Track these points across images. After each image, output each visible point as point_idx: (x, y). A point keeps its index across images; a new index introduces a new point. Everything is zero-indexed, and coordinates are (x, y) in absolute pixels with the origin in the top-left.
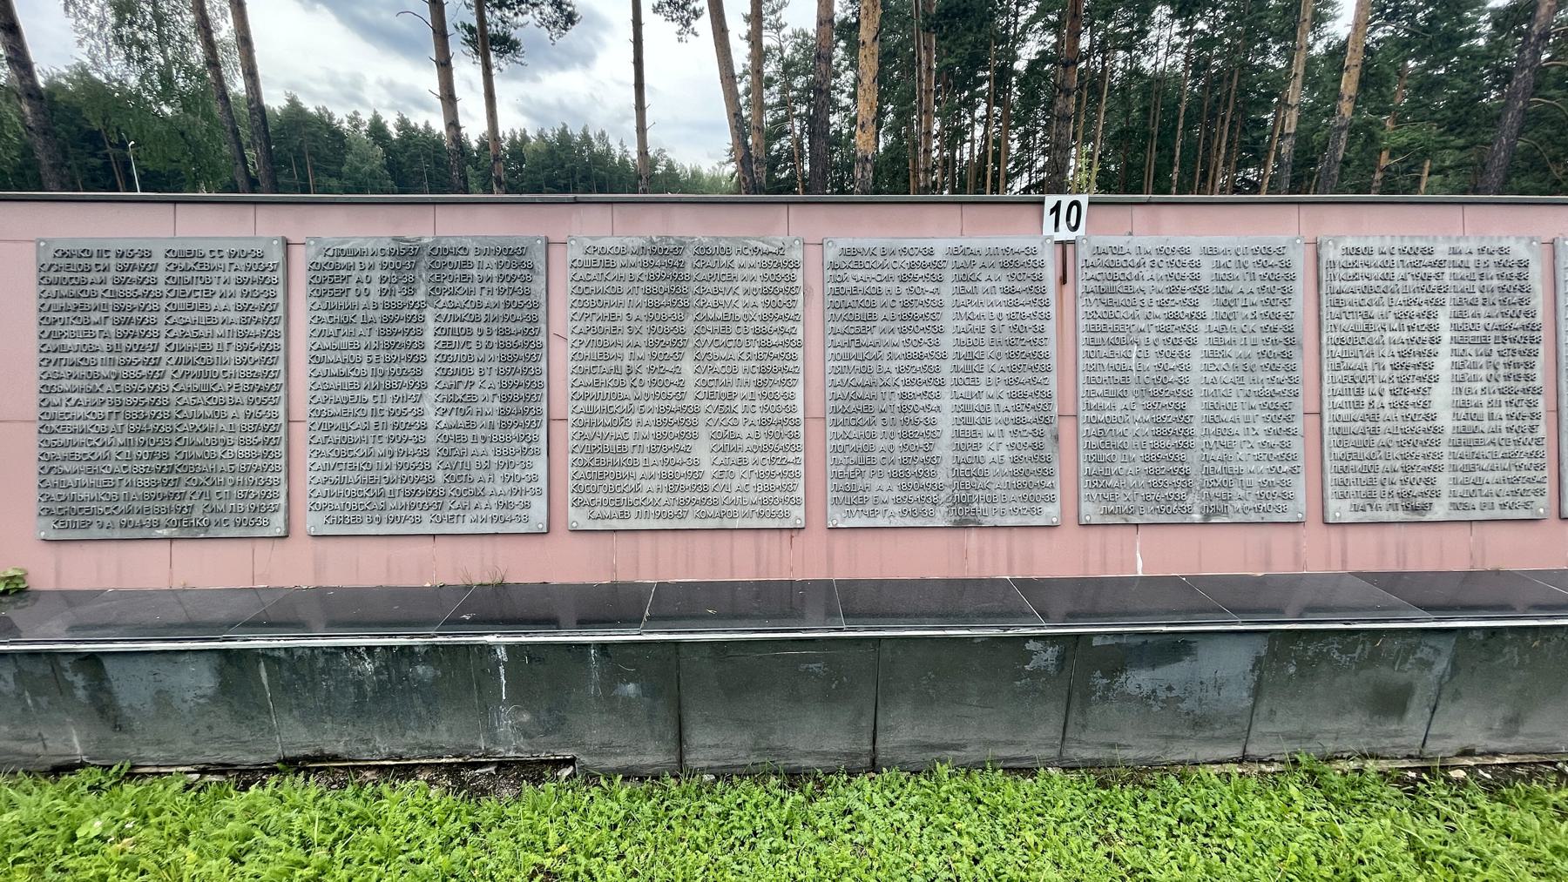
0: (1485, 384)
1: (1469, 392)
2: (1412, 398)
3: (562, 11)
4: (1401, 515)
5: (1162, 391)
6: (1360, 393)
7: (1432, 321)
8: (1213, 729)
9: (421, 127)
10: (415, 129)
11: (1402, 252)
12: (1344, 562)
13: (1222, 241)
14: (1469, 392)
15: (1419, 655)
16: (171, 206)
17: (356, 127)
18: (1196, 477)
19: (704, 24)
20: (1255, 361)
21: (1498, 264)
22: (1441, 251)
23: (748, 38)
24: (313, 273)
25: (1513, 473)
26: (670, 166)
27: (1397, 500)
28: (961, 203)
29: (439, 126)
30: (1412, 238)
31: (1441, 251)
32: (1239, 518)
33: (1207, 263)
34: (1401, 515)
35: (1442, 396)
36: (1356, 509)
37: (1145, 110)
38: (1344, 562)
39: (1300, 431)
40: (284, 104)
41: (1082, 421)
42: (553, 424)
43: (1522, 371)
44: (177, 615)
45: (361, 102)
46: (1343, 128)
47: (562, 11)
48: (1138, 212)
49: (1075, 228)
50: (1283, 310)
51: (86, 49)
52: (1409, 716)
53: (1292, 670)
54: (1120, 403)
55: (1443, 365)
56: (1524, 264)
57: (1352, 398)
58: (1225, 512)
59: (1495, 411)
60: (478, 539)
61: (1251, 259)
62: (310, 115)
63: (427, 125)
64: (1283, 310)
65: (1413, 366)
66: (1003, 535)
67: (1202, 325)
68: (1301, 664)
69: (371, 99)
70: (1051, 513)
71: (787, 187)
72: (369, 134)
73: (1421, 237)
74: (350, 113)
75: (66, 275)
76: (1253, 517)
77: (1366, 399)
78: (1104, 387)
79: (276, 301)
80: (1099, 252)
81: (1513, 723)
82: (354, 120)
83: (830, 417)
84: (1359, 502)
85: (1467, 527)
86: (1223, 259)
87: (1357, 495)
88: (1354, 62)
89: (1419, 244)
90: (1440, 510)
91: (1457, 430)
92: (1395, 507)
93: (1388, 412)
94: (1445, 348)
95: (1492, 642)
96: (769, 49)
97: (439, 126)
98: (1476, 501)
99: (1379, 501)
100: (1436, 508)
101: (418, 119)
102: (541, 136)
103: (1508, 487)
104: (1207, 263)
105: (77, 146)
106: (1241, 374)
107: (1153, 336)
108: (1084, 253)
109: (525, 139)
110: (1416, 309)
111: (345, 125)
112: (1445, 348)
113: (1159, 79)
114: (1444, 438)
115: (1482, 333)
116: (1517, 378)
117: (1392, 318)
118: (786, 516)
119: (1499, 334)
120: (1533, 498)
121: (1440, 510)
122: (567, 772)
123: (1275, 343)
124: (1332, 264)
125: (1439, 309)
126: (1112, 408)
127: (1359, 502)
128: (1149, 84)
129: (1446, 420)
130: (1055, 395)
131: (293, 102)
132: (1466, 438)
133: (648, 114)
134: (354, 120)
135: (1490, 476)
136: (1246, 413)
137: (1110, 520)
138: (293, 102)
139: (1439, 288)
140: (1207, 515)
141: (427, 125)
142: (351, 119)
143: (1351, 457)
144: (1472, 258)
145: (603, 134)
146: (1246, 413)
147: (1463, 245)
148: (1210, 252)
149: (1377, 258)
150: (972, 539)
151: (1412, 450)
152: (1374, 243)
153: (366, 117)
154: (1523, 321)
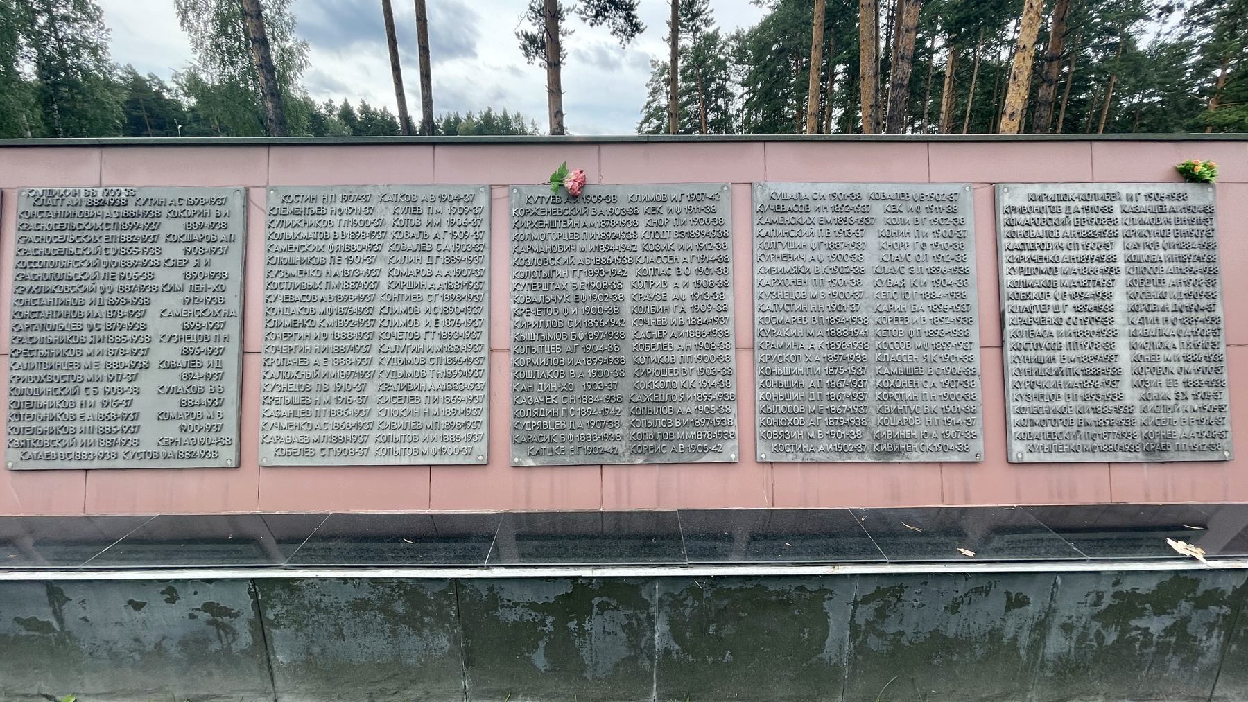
10: (375, 113)
17: (330, 112)
23: (669, 40)
24: (516, 256)
29: (394, 111)
39: (978, 371)
41: (486, 347)
42: (997, 343)
44: (1127, 522)
60: (221, 472)
74: (326, 101)
82: (329, 107)
85: (938, 467)
97: (394, 111)
101: (376, 106)
109: (457, 120)
111: (323, 111)
122: (1056, 644)
124: (1011, 209)
133: (565, 99)
134: (329, 107)
145: (518, 116)
151: (1093, 391)
153: (338, 103)
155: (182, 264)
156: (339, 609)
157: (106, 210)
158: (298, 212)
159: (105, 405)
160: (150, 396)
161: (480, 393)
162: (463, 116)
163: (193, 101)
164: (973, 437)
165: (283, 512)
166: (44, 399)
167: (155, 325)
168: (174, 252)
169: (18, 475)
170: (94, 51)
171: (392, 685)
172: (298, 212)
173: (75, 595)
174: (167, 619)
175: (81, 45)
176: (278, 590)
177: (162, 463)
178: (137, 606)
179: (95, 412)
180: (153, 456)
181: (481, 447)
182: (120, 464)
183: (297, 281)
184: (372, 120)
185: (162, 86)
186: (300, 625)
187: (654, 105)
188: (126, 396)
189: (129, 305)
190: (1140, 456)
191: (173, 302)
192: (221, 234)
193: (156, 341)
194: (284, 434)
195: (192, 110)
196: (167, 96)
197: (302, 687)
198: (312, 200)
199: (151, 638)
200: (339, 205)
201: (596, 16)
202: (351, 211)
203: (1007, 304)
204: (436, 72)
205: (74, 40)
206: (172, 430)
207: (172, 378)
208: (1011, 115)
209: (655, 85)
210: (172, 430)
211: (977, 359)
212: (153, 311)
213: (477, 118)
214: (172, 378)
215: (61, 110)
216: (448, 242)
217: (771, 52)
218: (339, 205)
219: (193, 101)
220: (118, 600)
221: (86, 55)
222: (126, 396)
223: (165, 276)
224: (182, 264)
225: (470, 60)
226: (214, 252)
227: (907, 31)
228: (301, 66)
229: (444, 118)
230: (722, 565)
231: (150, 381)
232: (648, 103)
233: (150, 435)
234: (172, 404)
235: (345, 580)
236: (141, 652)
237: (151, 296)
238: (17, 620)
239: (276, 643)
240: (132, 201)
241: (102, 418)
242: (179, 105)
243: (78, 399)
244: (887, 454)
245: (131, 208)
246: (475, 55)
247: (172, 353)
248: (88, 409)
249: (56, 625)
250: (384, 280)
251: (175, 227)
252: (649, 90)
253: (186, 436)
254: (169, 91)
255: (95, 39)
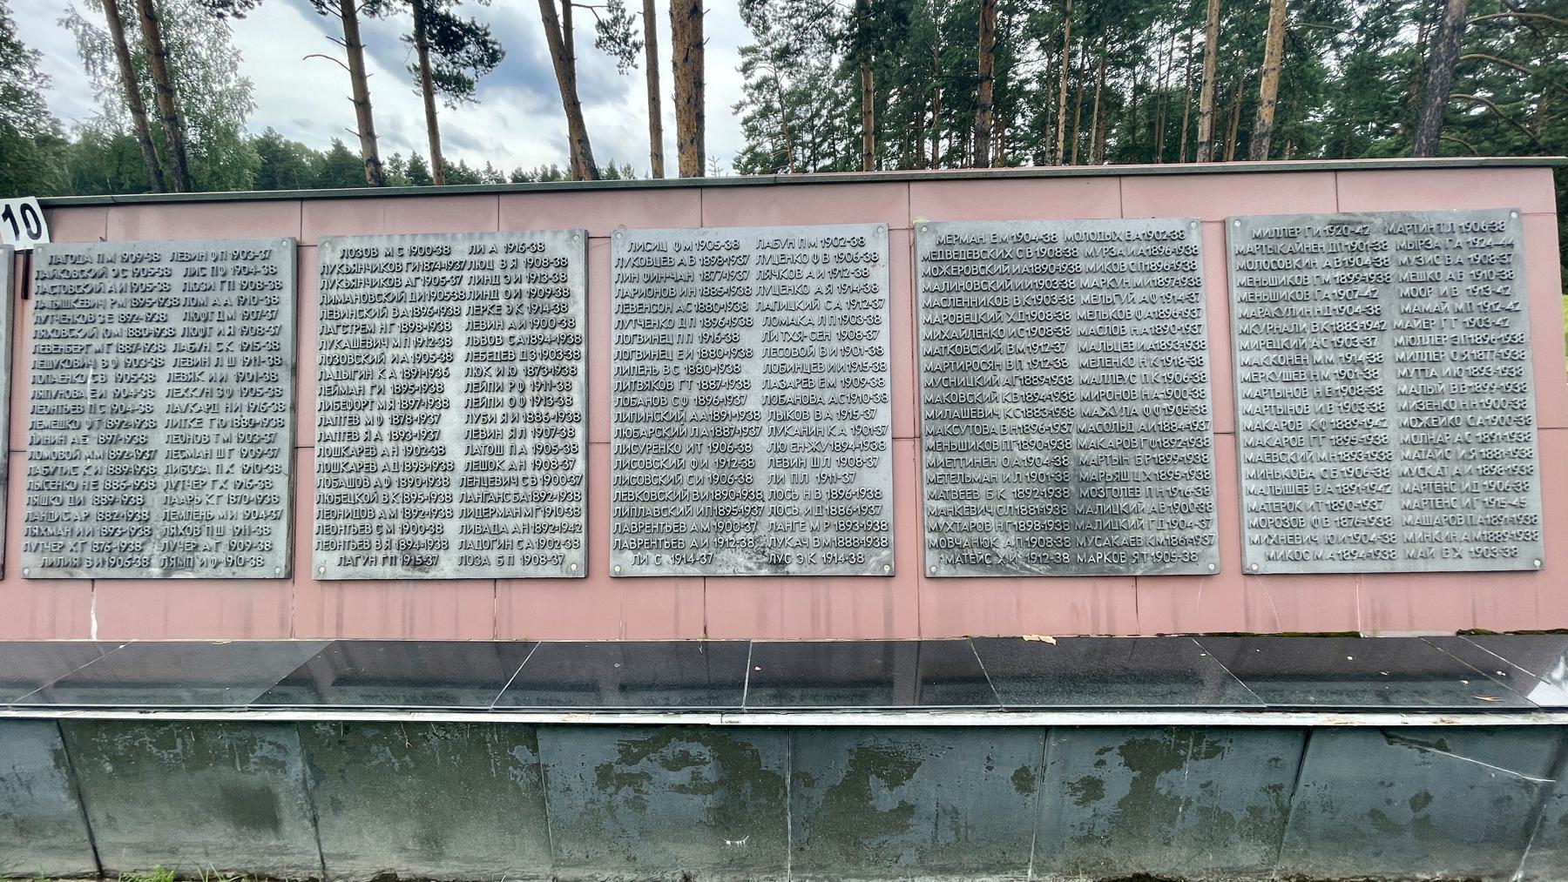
0: (507, 409)
1: (487, 420)
2: (416, 428)
3: (486, 49)
4: (400, 571)
5: (120, 422)
6: (354, 421)
7: (444, 335)
8: (45, 837)
9: (457, 165)
11: (413, 253)
12: (339, 627)
13: (194, 245)
14: (487, 420)
15: (259, 753)
17: (397, 167)
18: (158, 524)
19: (641, 57)
20: (232, 384)
21: (530, 264)
22: (460, 253)
25: (540, 520)
27: (395, 552)
30: (425, 236)
31: (460, 253)
32: (207, 572)
33: (179, 269)
34: (400, 571)
35: (452, 424)
36: (344, 562)
37: (1151, 126)
38: (339, 627)
40: (331, 149)
42: (593, 448)
43: (555, 394)
45: (404, 143)
46: (1264, 135)
47: (486, 49)
48: (114, 214)
49: (38, 236)
51: (102, 103)
52: (287, 828)
53: (109, 768)
54: (71, 435)
55: (455, 389)
56: (563, 264)
57: (346, 429)
58: (189, 565)
59: (519, 443)
61: (229, 265)
62: (354, 158)
63: (462, 165)
65: (418, 395)
67: (170, 344)
68: (114, 760)
69: (411, 140)
72: (409, 174)
73: (436, 235)
74: (392, 156)
76: (224, 572)
77: (362, 429)
78: (53, 418)
80: (54, 261)
81: (432, 843)
82: (395, 162)
83: (887, 439)
84: (350, 554)
86: (196, 265)
87: (346, 545)
88: (1272, 65)
89: (433, 243)
90: (448, 566)
91: (470, 467)
92: (393, 561)
93: (387, 445)
94: (458, 368)
95: (350, 738)
96: (1019, 91)
98: (493, 555)
99: (374, 553)
100: (442, 563)
103: (533, 538)
104: (179, 269)
106: (214, 401)
107: (112, 356)
108: (39, 264)
110: (425, 321)
112: (458, 368)
113: (1164, 95)
114: (456, 477)
116: (547, 401)
117: (396, 332)
119: (529, 348)
120: (563, 550)
121: (448, 566)
123: (257, 362)
125: (453, 320)
126: (62, 442)
127: (350, 554)
128: (1154, 99)
129: (457, 454)
131: (339, 147)
132: (480, 475)
135: (511, 523)
136: (221, 446)
137: (51, 573)
138: (339, 147)
140: (170, 566)
141: (462, 165)
142: (392, 161)
143: (339, 500)
144: (497, 258)
146: (221, 446)
147: (488, 243)
148: (181, 258)
149: (382, 260)
152: (381, 245)
153: (406, 158)
154: (559, 331)
161: (576, 489)
164: (1206, 542)
165: (225, 641)
169: (618, 582)
173: (544, 740)
181: (575, 558)
203: (287, 416)
204: (589, 115)
211: (1534, 438)
225: (621, 106)
230: (1113, 710)
235: (348, 725)
246: (625, 102)
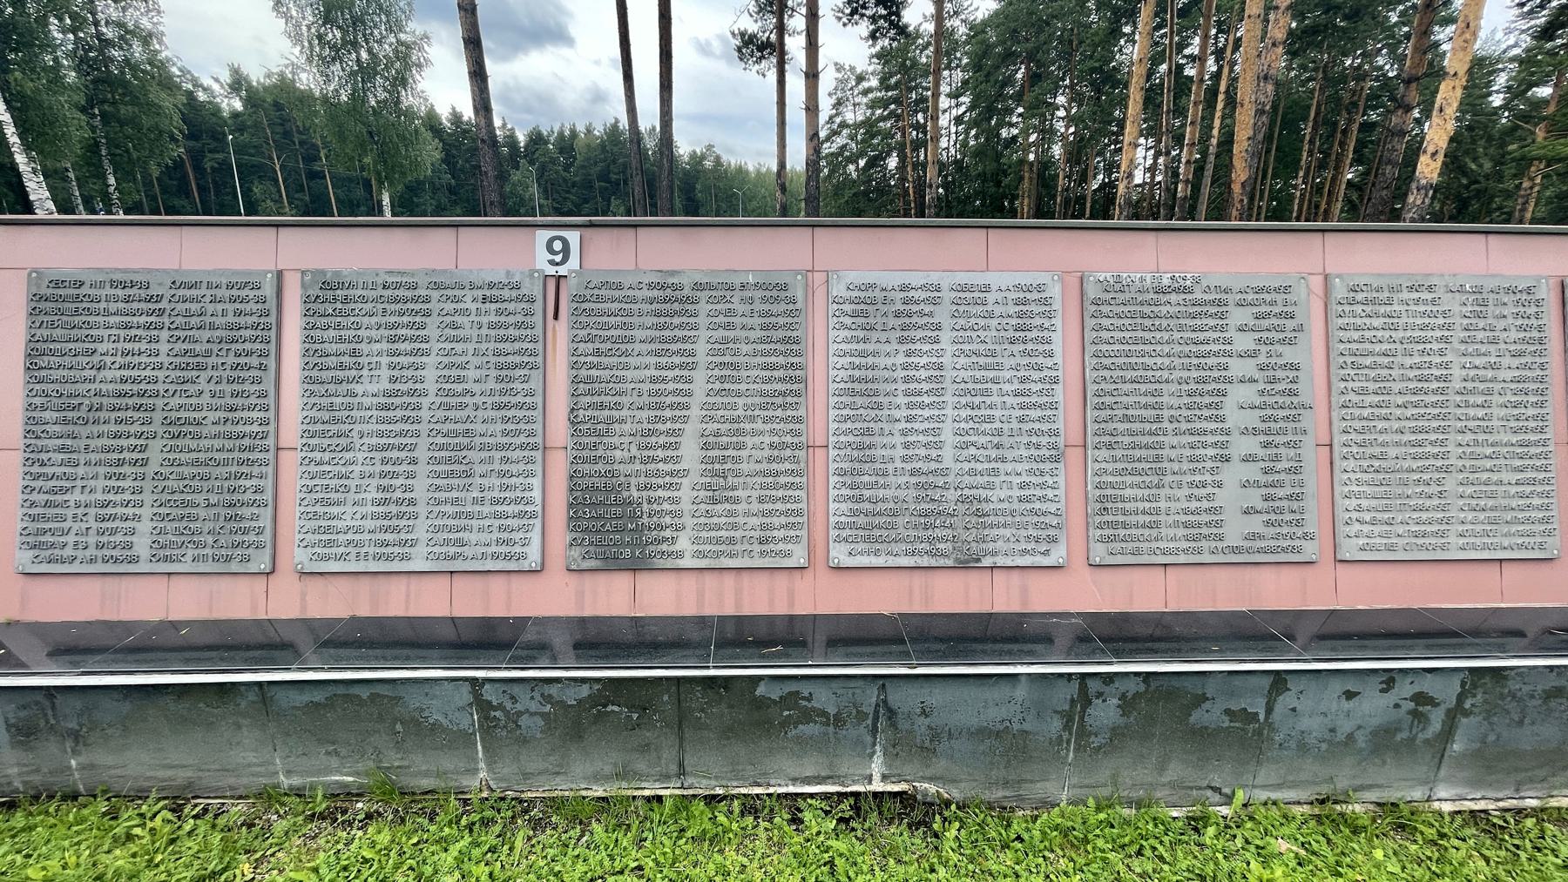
16: (274, 230)
26: (718, 160)
28: (1324, 231)
50: (1535, 323)
64: (1535, 323)
66: (1015, 575)
70: (1057, 555)
71: (1104, 205)
75: (56, 304)
79: (534, 319)
97: (468, 113)
102: (589, 131)
105: (165, 156)
109: (574, 134)
115: (998, 425)
118: (788, 555)
130: (1062, 433)
139: (1434, 300)
150: (974, 580)
155: (1253, 354)
156: (1532, 697)
157: (1173, 298)
158: (1366, 302)
159: (1189, 497)
160: (1233, 490)
162: (581, 128)
163: (238, 105)
166: (1128, 492)
167: (1235, 418)
168: (1244, 342)
170: (146, 40)
171: (1542, 773)
172: (1366, 302)
174: (1374, 707)
175: (128, 34)
176: (1487, 679)
177: (1242, 561)
178: (1350, 695)
179: (1179, 505)
180: (1235, 550)
182: (1207, 558)
183: (1373, 374)
184: (465, 131)
185: (197, 85)
186: (1488, 715)
187: (838, 120)
188: (1209, 490)
189: (1207, 393)
190: (950, 563)
191: (1247, 393)
192: (1290, 324)
193: (1236, 433)
194: (1366, 529)
195: (235, 115)
196: (202, 96)
197: (1465, 774)
198: (1379, 289)
199: (1346, 727)
200: (1405, 295)
201: (852, 14)
202: (1417, 302)
205: (120, 25)
206: (1256, 524)
207: (1253, 472)
208: (1434, 154)
209: (839, 94)
210: (1256, 524)
212: (1229, 404)
213: (598, 131)
214: (1253, 472)
215: (103, 115)
216: (1514, 335)
217: (1002, 62)
218: (1405, 295)
219: (238, 105)
220: (1337, 687)
221: (137, 50)
222: (1209, 490)
223: (1238, 368)
224: (1253, 354)
225: (565, 51)
226: (1282, 342)
227: (1274, 45)
228: (419, 66)
229: (556, 130)
231: (1234, 474)
232: (831, 118)
233: (1235, 530)
234: (1255, 498)
235: (1551, 668)
236: (1330, 743)
237: (1228, 386)
238: (1228, 712)
239: (1459, 732)
240: (1197, 289)
241: (1186, 512)
242: (216, 111)
243: (1163, 492)
244: (968, 564)
245: (1198, 295)
247: (1251, 445)
248: (1174, 501)
249: (1262, 717)
250: (1457, 372)
251: (1239, 316)
252: (833, 100)
253: (1272, 531)
254: (205, 89)
255: (145, 23)
